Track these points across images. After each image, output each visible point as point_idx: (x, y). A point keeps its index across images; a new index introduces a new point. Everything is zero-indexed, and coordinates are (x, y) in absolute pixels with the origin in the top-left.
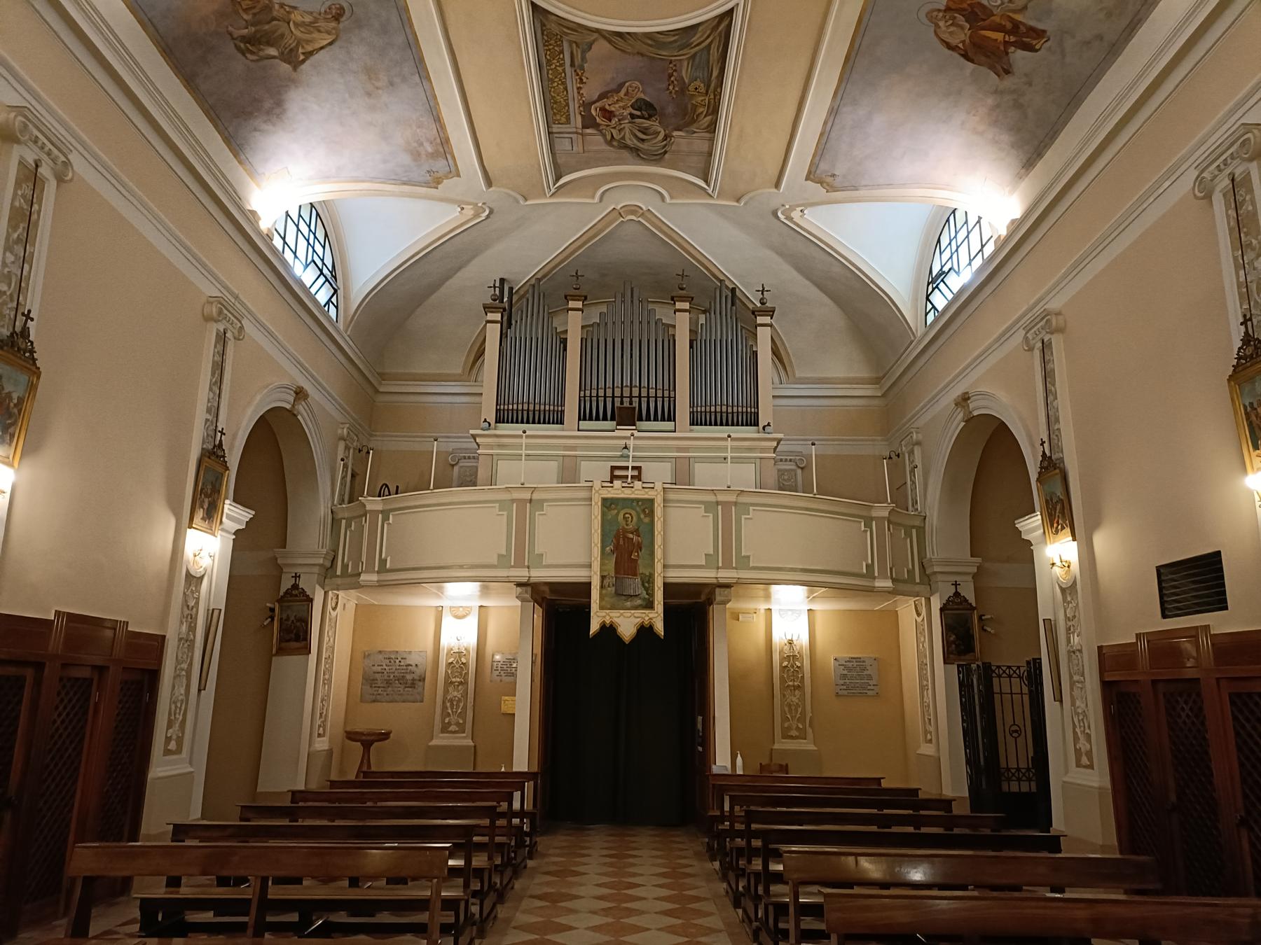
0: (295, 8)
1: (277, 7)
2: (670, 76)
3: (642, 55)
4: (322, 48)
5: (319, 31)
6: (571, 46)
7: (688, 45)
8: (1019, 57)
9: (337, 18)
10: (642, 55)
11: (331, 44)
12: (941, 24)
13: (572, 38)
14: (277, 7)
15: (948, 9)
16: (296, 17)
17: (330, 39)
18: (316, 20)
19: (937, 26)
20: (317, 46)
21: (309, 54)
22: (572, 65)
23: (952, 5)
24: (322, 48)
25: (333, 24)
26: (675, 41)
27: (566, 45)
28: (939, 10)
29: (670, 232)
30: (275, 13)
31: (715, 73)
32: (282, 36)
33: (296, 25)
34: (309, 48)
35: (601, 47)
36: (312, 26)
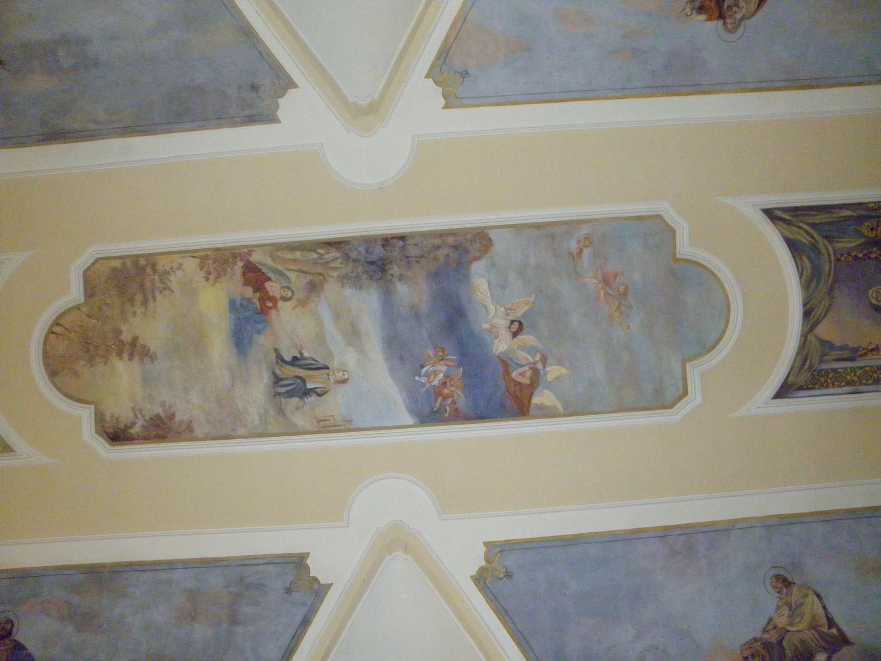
0: (770, 621)
1: (766, 636)
2: (856, 258)
3: (831, 290)
4: (824, 608)
5: (802, 604)
6: (827, 361)
7: (814, 247)
8: (203, 273)
9: (787, 583)
10: (831, 290)
11: (819, 596)
12: (739, 16)
13: (816, 361)
14: (766, 636)
15: (721, 16)
16: (782, 621)
17: (812, 598)
18: (789, 605)
19: (741, 20)
20: (821, 611)
21: (831, 623)
22: (852, 359)
23: (716, 14)
24: (824, 608)
25: (795, 589)
26: (809, 258)
27: (825, 366)
28: (725, 24)
29: (788, 400)
30: (774, 640)
31: (848, 213)
32: (802, 641)
33: (791, 624)
34: (824, 621)
35: (825, 330)
36: (794, 611)
